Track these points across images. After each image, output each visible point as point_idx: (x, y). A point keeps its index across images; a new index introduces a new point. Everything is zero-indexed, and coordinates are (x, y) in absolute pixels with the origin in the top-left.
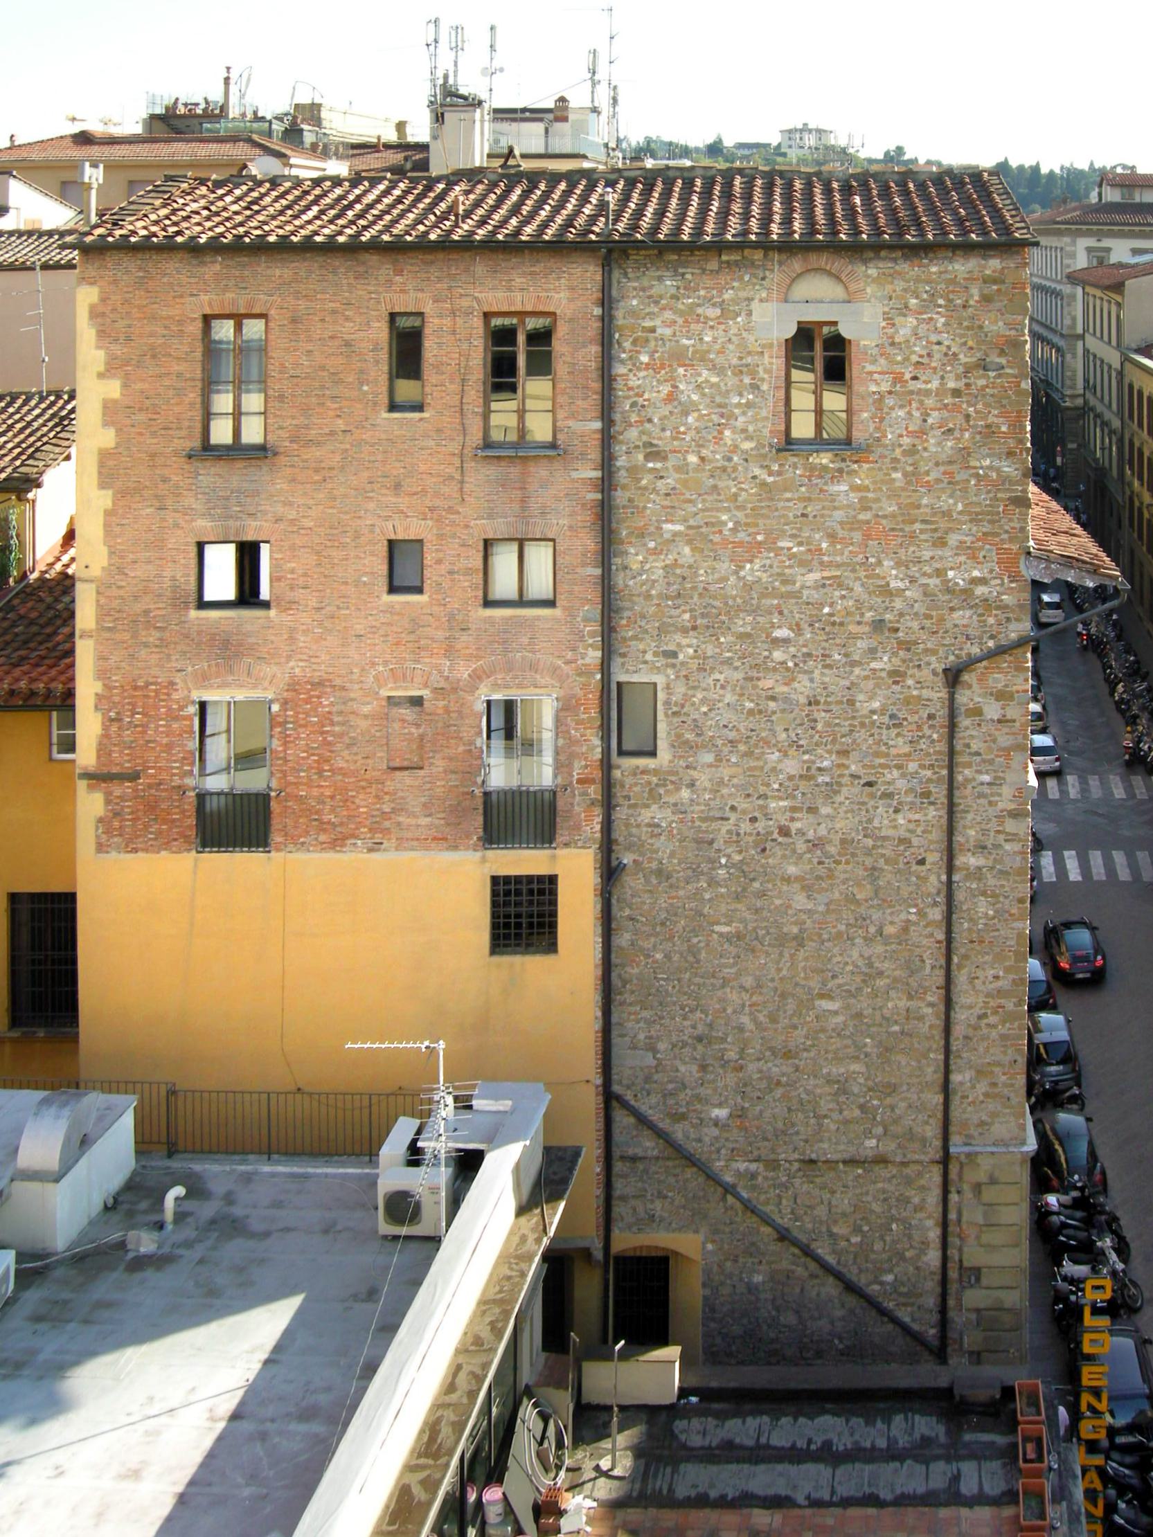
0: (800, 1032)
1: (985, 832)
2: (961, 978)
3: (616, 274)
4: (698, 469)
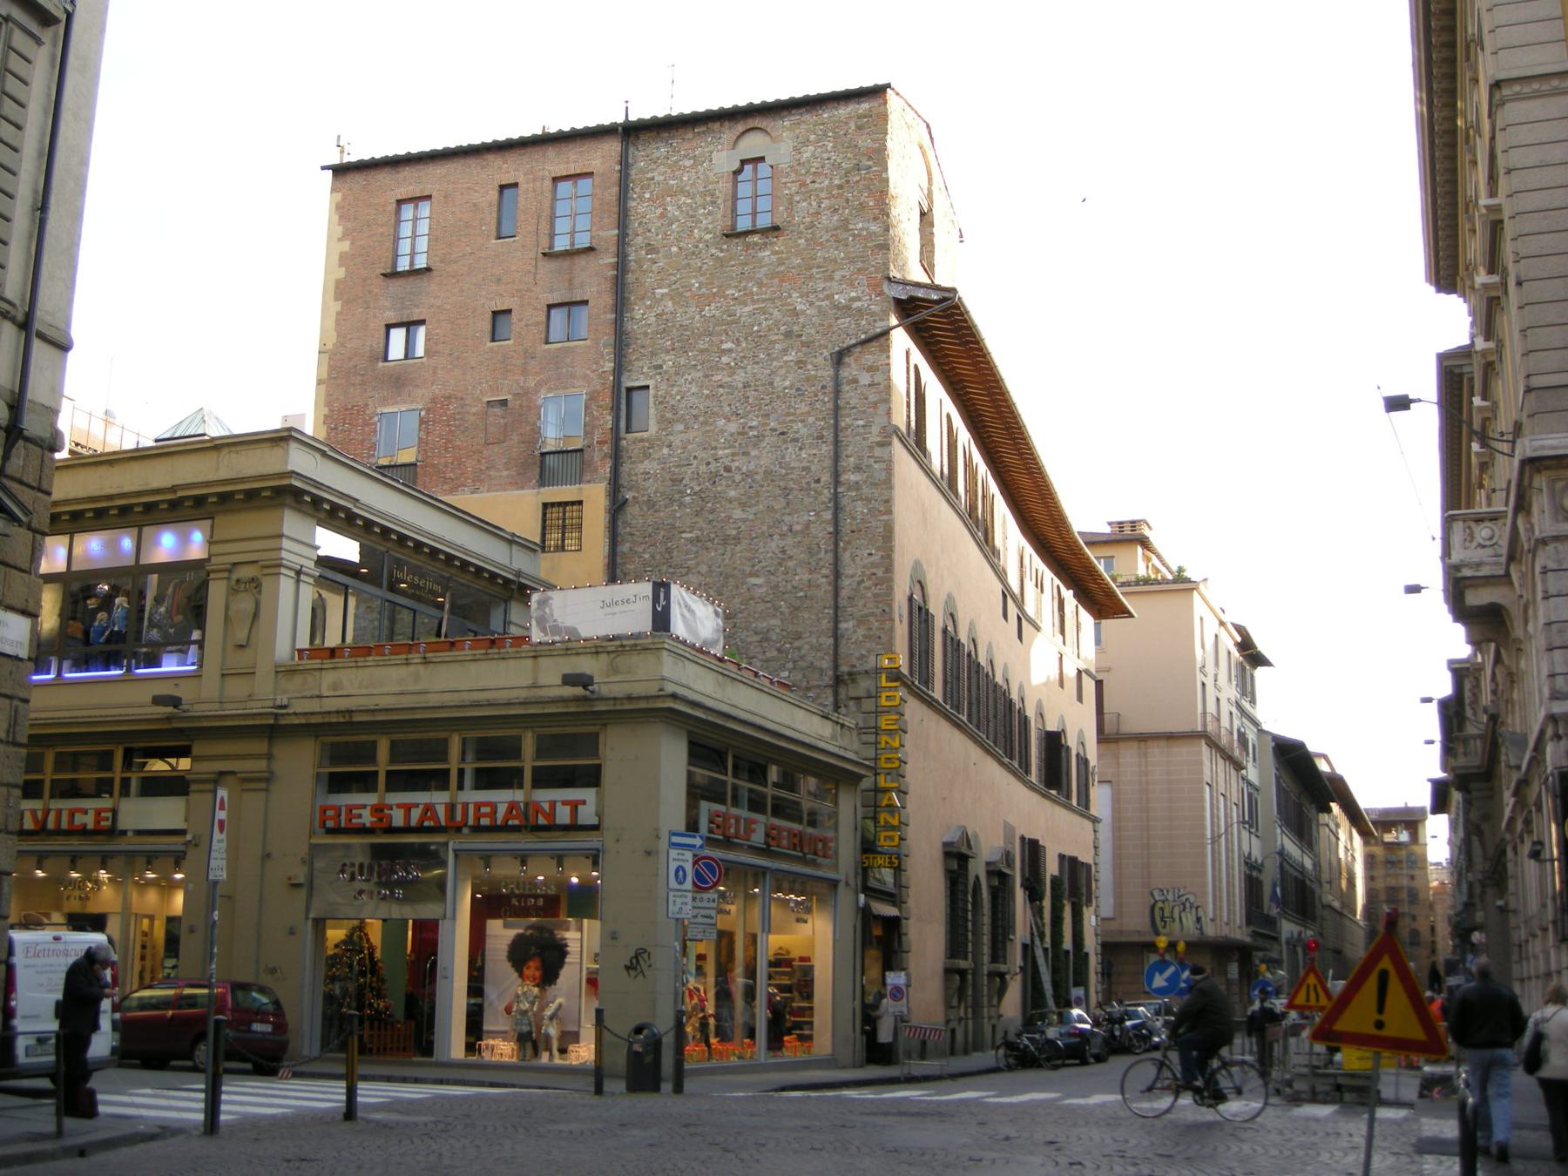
0: (737, 600)
1: (860, 458)
2: (846, 557)
3: (631, 150)
4: (677, 255)
